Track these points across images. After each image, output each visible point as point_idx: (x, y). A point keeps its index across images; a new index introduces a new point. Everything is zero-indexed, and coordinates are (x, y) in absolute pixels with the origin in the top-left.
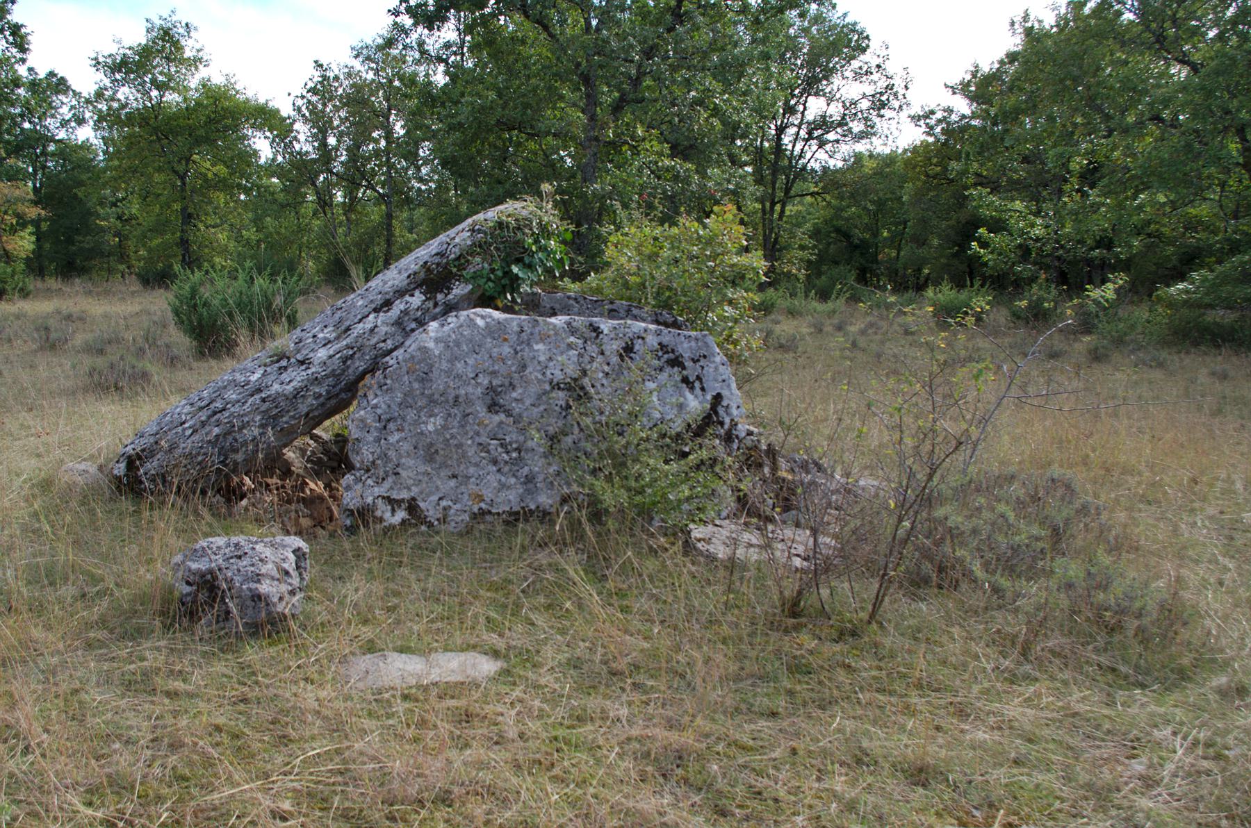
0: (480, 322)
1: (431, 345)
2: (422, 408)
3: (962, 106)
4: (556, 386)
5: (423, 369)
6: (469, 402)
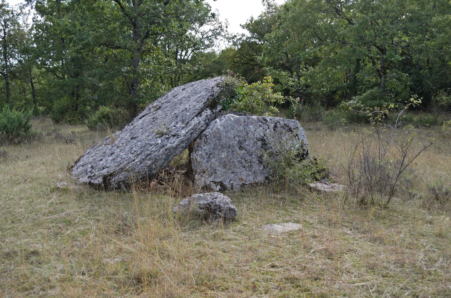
0: (232, 119)
1: (219, 127)
2: (219, 150)
3: (248, 34)
4: (258, 140)
5: (218, 136)
6: (233, 146)
